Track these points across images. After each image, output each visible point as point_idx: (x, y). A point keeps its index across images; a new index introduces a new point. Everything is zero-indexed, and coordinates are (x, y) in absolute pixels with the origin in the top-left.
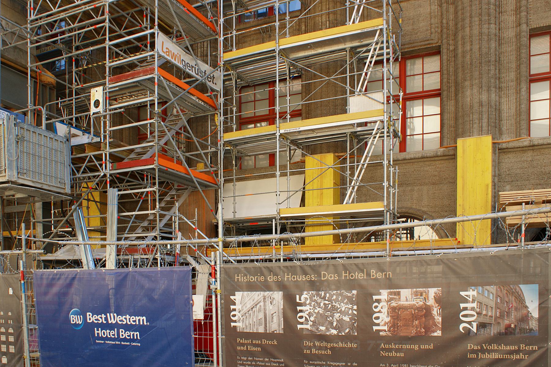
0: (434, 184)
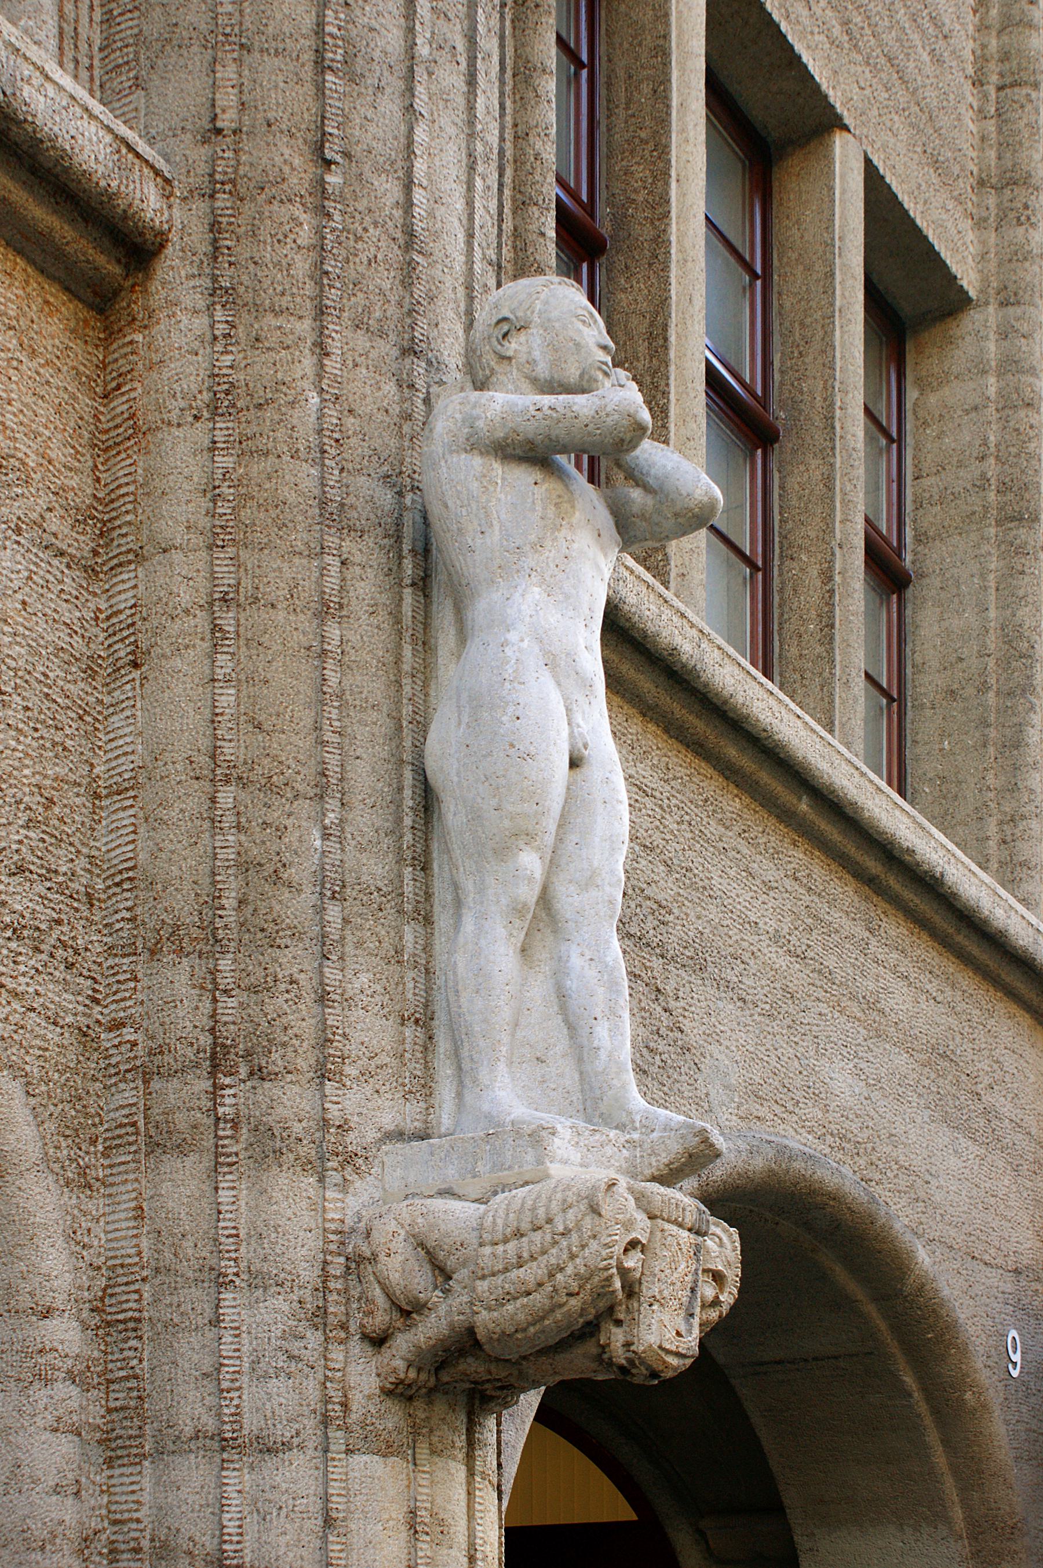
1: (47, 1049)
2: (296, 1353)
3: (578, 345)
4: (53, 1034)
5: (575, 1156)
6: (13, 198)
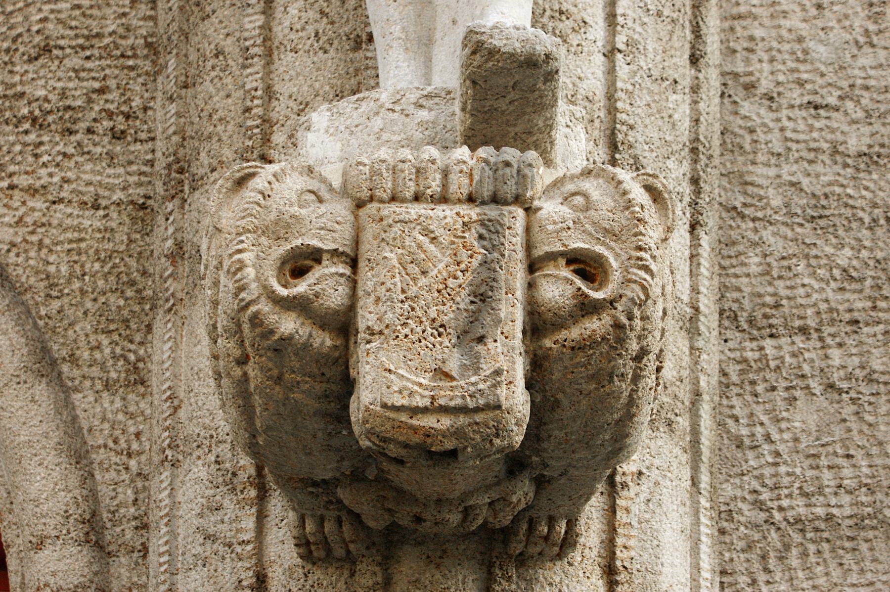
1: (81, 240)
2: (211, 531)
4: (91, 221)
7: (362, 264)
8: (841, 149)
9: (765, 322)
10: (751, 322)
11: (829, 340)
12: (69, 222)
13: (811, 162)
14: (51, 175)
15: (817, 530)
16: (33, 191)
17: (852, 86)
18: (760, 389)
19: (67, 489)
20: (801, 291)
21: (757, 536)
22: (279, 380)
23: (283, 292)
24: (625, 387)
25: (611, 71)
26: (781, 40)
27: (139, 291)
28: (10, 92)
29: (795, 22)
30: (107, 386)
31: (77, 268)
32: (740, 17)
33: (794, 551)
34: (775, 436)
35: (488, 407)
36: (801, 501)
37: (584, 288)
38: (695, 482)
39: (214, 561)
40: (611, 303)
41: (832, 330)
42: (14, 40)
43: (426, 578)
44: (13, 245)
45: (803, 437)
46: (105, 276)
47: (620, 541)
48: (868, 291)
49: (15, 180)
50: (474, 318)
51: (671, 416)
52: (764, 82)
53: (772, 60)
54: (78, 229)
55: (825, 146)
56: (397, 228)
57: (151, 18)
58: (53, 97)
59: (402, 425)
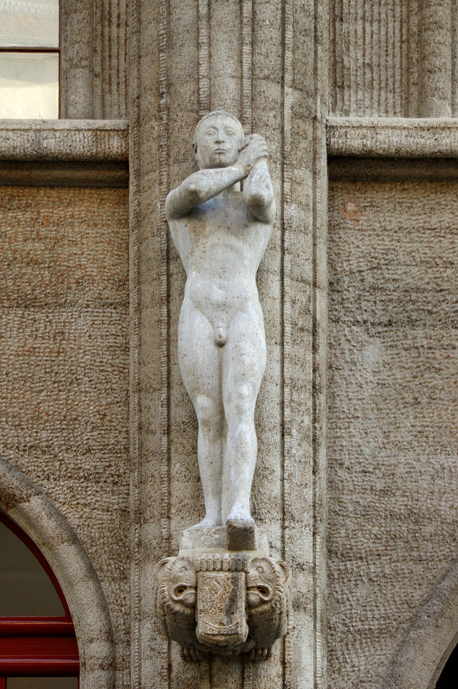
0: (28, 303)
1: (103, 524)
2: (153, 647)
3: (206, 147)
4: (106, 516)
5: (190, 544)
6: (66, 176)
7: (198, 590)
8: (374, 488)
9: (347, 555)
10: (342, 555)
11: (370, 562)
12: (98, 516)
13: (363, 493)
14: (92, 499)
15: (365, 634)
16: (85, 505)
17: (378, 464)
18: (345, 580)
19: (100, 621)
20: (360, 543)
21: (344, 637)
22: (175, 621)
23: (176, 598)
24: (277, 622)
25: (283, 486)
26: (352, 446)
27: (124, 543)
28: (76, 467)
29: (357, 439)
30: (113, 580)
31: (102, 535)
32: (337, 437)
33: (358, 642)
34: (351, 599)
35: (235, 634)
36: (360, 623)
37: (262, 597)
38: (315, 627)
39: (154, 658)
40: (270, 601)
41: (371, 558)
42: (78, 447)
43: (223, 668)
44: (79, 526)
45: (361, 599)
46: (112, 537)
47: (286, 653)
48: (384, 543)
49: (79, 501)
50: (231, 607)
51: (305, 606)
52: (346, 463)
53: (349, 454)
54: (101, 519)
55: (368, 487)
56: (208, 580)
57: (126, 438)
58: (92, 469)
59: (210, 639)
